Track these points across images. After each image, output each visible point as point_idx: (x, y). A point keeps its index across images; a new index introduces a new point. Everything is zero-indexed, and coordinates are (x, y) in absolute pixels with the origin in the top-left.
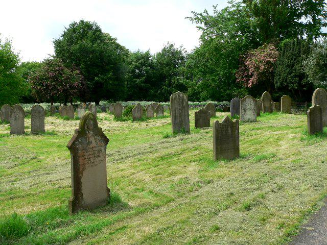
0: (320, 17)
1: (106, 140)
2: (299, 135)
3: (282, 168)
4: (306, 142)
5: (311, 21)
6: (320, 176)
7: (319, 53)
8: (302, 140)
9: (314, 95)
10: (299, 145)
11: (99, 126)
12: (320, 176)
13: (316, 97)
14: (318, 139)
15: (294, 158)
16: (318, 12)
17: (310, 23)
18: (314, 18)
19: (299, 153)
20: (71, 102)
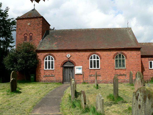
0: (9, 39)
1: (50, 25)
2: (6, 93)
3: (4, 108)
4: (10, 96)
5: (5, 40)
6: (22, 110)
7: (11, 55)
8: (8, 94)
9: (11, 74)
10: (7, 97)
11: (139, 42)
12: (22, 110)
13: (12, 75)
14: (15, 94)
15: (7, 103)
16: (8, 37)
17: (4, 41)
18: (6, 39)
19: (9, 101)
20: (142, 95)
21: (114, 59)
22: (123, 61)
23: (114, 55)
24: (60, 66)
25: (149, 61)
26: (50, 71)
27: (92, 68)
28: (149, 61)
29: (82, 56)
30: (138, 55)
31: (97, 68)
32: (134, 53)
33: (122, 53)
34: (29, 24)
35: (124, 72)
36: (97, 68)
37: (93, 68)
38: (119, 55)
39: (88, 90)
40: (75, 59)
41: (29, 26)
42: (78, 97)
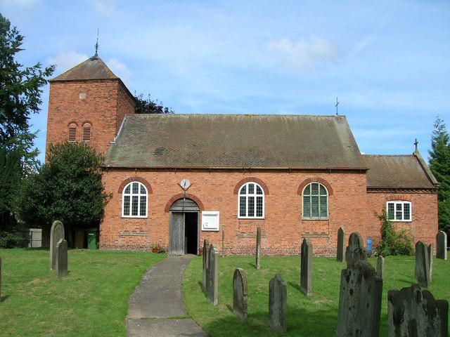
23: (301, 187)
32: (352, 179)
33: (322, 181)
34: (82, 96)
35: (325, 228)
37: (247, 217)
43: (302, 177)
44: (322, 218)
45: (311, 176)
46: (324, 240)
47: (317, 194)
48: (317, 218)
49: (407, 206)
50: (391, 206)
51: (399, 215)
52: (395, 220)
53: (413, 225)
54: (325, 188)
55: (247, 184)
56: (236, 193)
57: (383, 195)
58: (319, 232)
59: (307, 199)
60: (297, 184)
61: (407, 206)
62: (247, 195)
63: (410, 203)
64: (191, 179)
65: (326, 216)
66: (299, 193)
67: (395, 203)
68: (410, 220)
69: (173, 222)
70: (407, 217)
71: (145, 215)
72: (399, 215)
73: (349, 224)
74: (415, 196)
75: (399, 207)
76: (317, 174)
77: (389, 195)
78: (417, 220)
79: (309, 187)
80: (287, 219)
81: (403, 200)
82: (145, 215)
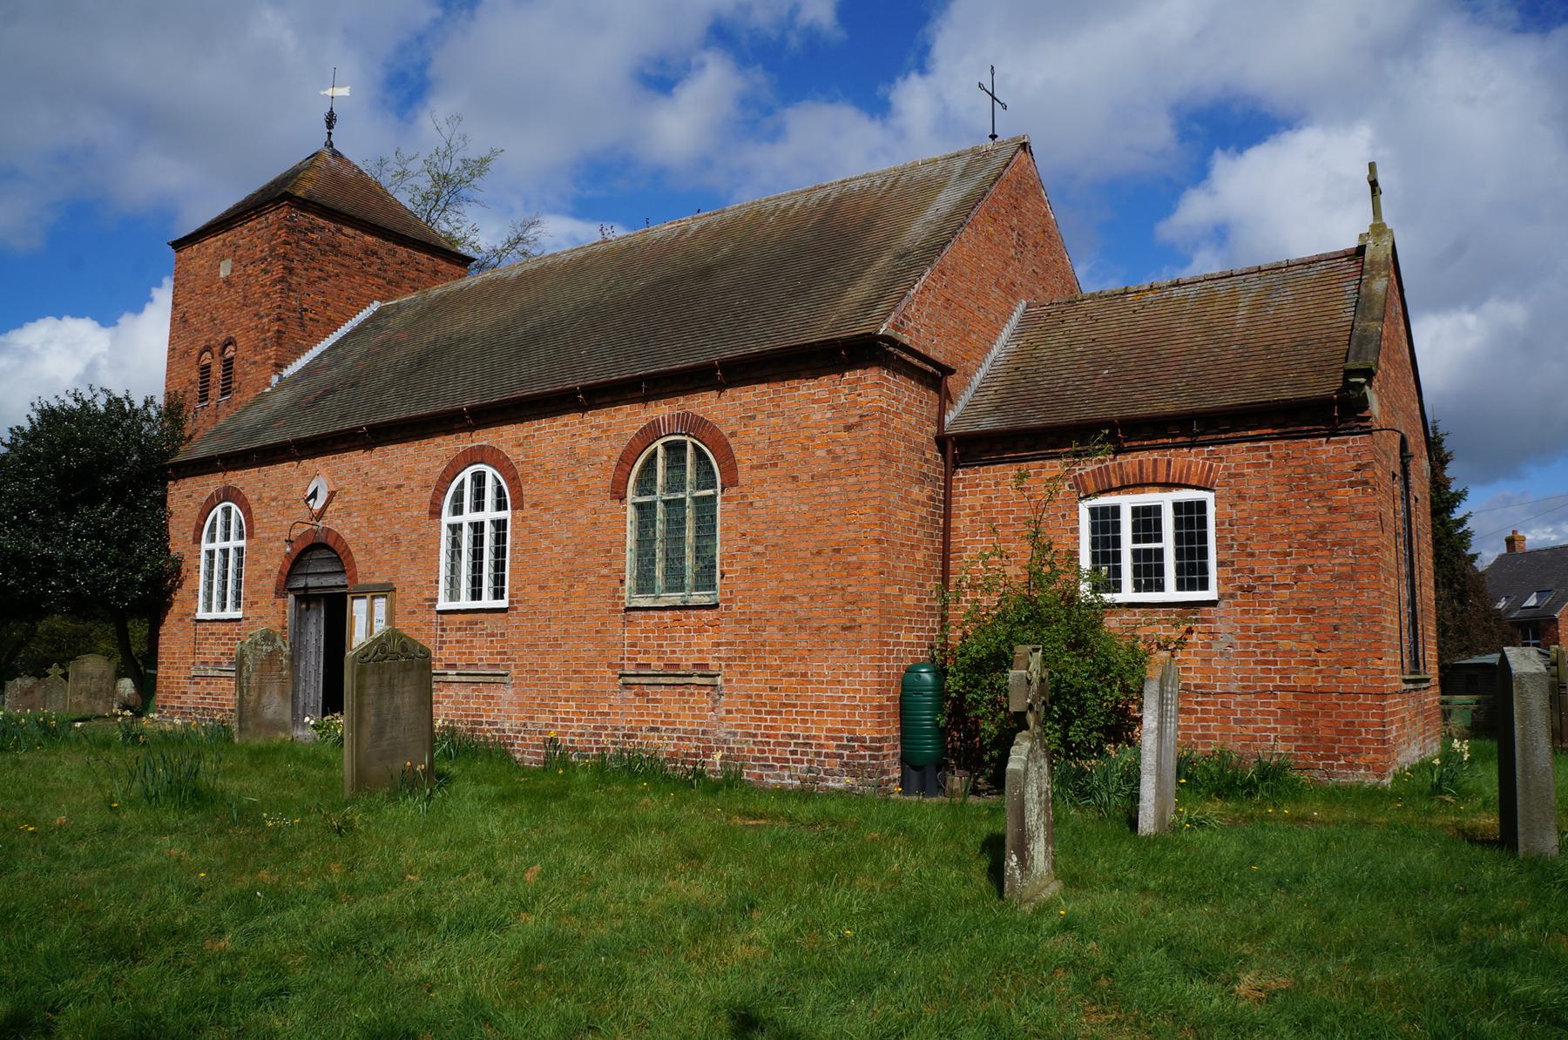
21: (622, 498)
22: (705, 507)
23: (626, 461)
24: (270, 584)
25: (1084, 509)
26: (227, 627)
27: (1160, 587)
28: (1084, 509)
29: (400, 486)
30: (848, 428)
31: (1180, 587)
32: (812, 400)
33: (696, 426)
34: (225, 270)
35: (706, 640)
36: (1138, 587)
37: (1171, 594)
38: (668, 447)
39: (152, 847)
40: (356, 520)
41: (227, 281)
42: (1139, 720)
43: (628, 419)
44: (698, 598)
45: (661, 410)
46: (702, 699)
47: (683, 488)
48: (675, 598)
49: (1190, 515)
50: (1105, 521)
51: (1148, 572)
52: (1127, 594)
53: (1225, 623)
54: (713, 457)
55: (467, 475)
56: (436, 513)
57: (1055, 467)
58: (687, 661)
59: (645, 510)
60: (611, 451)
61: (1190, 515)
62: (468, 516)
63: (1209, 497)
64: (333, 475)
65: (712, 587)
66: (619, 494)
67: (1127, 503)
68: (1211, 594)
69: (300, 620)
70: (1192, 575)
71: (1204, 586)
72: (1148, 572)
73: (802, 624)
74: (1237, 455)
75: (1147, 521)
76: (682, 400)
77: (1089, 467)
78: (1245, 590)
79: (654, 454)
80: (575, 606)
81: (1168, 486)
82: (1204, 586)
